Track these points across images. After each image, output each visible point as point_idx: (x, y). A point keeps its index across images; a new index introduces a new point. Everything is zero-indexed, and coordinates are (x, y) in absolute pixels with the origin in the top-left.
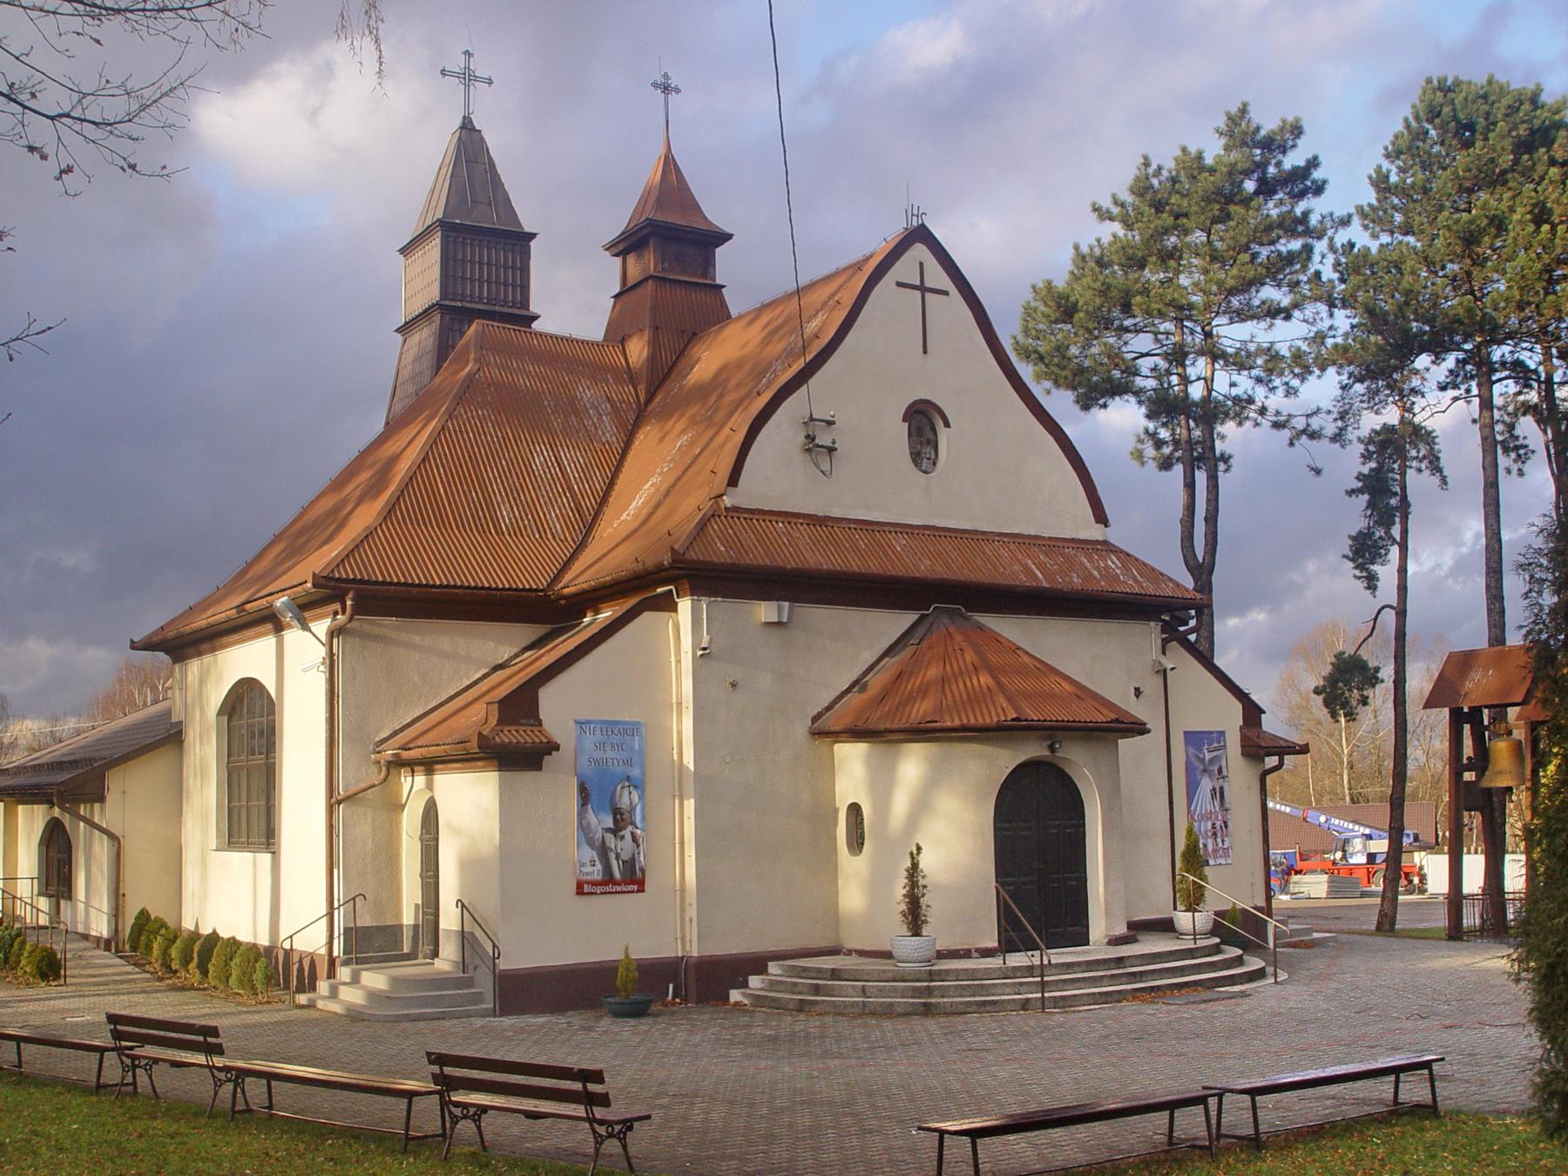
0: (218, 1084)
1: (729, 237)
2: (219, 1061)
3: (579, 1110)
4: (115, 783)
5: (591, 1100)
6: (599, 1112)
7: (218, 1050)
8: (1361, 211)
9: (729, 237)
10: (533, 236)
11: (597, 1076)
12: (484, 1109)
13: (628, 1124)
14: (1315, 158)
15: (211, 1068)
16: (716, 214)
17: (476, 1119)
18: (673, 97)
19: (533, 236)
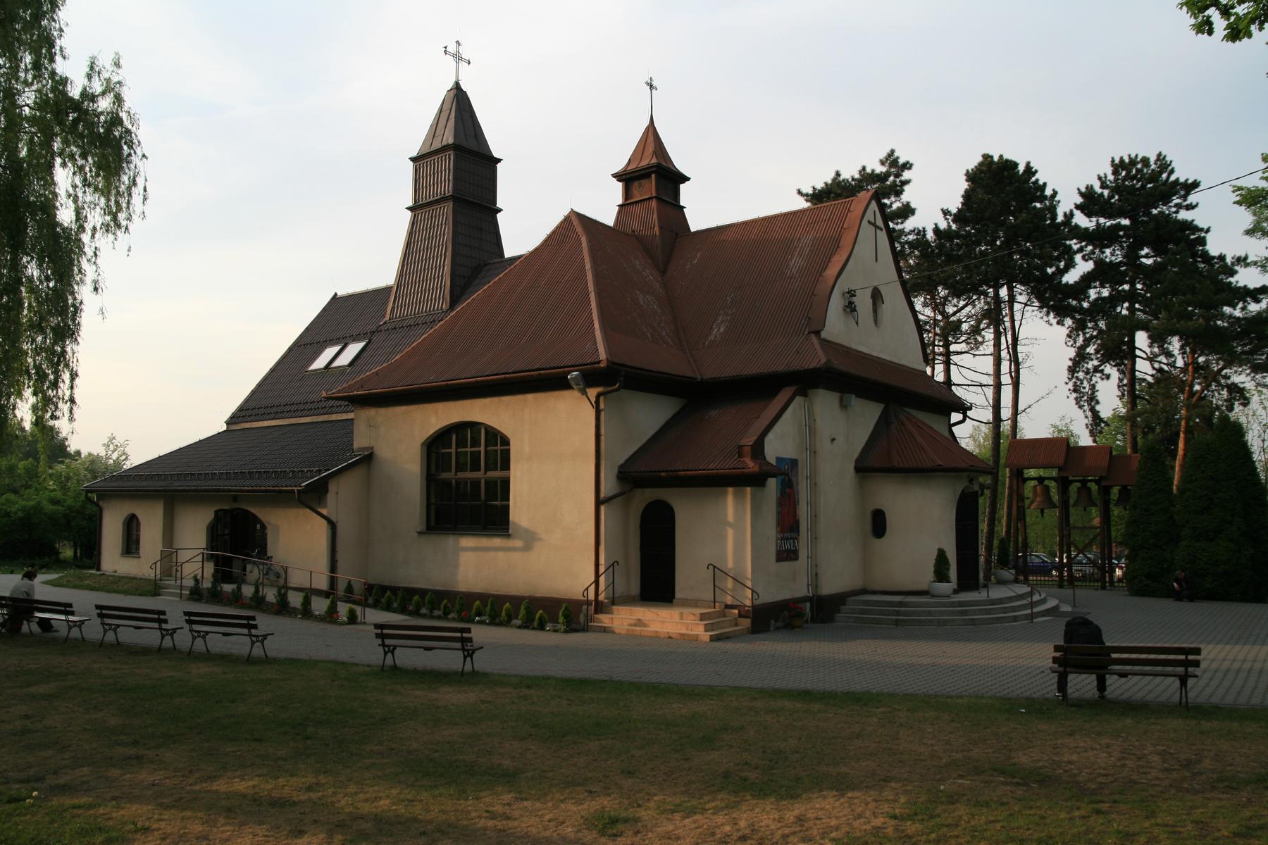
0: (70, 628)
1: (688, 179)
2: (71, 618)
3: (245, 631)
4: (332, 486)
5: (160, 621)
6: (254, 632)
7: (72, 613)
8: (1077, 207)
9: (688, 179)
10: (499, 160)
11: (163, 613)
12: (207, 633)
13: (265, 637)
14: (911, 165)
15: (68, 621)
16: (681, 164)
17: (204, 637)
18: (463, 65)
19: (499, 160)
